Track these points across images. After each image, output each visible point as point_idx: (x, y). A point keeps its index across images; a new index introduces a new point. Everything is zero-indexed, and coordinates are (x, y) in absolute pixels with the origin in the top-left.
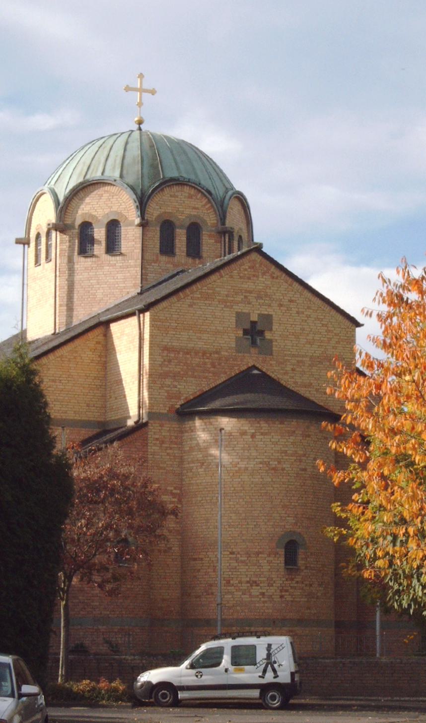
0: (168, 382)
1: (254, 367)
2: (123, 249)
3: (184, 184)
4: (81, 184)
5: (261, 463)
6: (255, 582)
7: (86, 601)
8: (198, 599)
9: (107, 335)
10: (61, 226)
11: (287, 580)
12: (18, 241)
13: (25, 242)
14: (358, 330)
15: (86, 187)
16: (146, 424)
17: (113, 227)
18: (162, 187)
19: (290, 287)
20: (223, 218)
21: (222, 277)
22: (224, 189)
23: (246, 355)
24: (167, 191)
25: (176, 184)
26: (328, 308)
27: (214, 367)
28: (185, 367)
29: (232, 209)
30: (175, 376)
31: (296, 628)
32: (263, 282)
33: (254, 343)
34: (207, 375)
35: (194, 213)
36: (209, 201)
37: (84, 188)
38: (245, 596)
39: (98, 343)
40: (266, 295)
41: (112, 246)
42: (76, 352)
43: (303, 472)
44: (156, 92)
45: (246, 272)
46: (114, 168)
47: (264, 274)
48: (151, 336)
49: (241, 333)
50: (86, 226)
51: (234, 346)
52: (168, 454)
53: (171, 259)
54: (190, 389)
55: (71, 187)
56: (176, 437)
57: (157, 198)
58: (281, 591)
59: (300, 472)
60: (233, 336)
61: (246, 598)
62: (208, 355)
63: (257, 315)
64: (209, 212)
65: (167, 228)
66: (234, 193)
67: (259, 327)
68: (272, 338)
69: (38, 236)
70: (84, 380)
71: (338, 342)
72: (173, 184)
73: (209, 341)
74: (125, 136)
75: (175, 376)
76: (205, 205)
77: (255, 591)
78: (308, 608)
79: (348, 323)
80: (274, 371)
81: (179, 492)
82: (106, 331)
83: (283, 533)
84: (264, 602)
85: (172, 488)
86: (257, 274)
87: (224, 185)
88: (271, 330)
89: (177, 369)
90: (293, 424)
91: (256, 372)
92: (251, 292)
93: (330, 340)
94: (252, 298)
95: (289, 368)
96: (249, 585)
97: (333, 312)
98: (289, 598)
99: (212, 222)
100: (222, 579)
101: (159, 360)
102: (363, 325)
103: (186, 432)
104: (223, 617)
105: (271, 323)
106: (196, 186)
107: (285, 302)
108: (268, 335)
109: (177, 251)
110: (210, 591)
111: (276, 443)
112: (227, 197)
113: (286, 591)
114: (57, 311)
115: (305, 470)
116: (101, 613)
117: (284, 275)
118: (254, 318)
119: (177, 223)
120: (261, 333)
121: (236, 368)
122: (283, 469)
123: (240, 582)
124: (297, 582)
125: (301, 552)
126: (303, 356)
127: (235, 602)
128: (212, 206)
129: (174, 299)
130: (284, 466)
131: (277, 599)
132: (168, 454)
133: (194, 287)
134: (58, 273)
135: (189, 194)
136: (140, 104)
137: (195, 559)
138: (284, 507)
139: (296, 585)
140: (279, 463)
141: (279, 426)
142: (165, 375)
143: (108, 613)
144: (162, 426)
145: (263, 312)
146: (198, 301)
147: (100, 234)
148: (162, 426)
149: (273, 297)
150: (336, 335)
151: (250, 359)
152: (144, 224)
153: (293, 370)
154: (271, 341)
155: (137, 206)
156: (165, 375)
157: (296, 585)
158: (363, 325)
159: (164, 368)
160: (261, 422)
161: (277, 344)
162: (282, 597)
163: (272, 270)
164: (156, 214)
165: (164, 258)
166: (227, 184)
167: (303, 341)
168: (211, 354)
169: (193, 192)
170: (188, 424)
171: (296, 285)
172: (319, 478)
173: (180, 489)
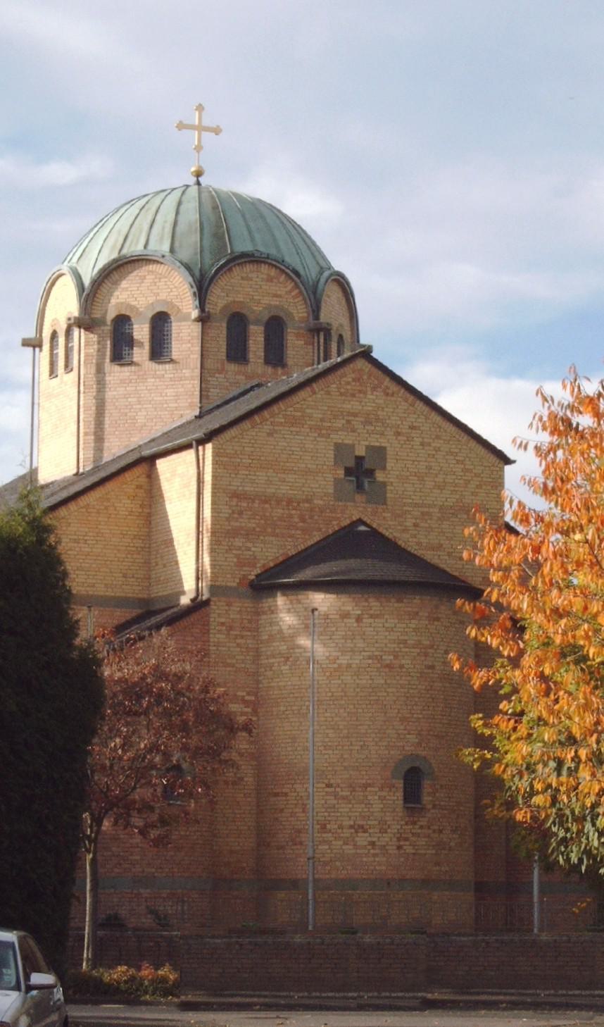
0: (238, 542)
1: (360, 522)
2: (175, 354)
3: (261, 262)
4: (115, 261)
5: (370, 658)
6: (362, 827)
8: (281, 851)
9: (152, 476)
10: (86, 321)
11: (406, 824)
12: (26, 343)
13: (35, 344)
14: (507, 468)
17: (160, 322)
19: (411, 408)
20: (316, 310)
21: (314, 393)
22: (317, 269)
24: (237, 271)
28: (263, 522)
30: (249, 534)
32: (373, 400)
33: (360, 487)
34: (293, 532)
35: (275, 302)
36: (296, 286)
37: (119, 267)
38: (347, 847)
40: (377, 420)
41: (159, 350)
42: (108, 500)
45: (349, 387)
46: (161, 239)
48: (214, 477)
49: (341, 473)
50: (122, 322)
52: (238, 645)
53: (242, 368)
54: (269, 552)
55: (100, 265)
56: (250, 621)
57: (223, 282)
58: (399, 840)
59: (425, 671)
60: (330, 477)
61: (349, 849)
62: (295, 504)
64: (296, 300)
65: (237, 323)
67: (367, 465)
68: (386, 480)
69: (54, 335)
70: (119, 540)
71: (479, 487)
72: (245, 262)
73: (297, 484)
74: (177, 194)
75: (249, 534)
76: (290, 292)
77: (362, 839)
78: (437, 864)
79: (493, 459)
80: (389, 526)
81: (253, 698)
84: (375, 855)
85: (245, 694)
86: (364, 389)
87: (318, 263)
88: (384, 468)
91: (362, 528)
92: (355, 415)
94: (357, 423)
95: (409, 523)
96: (353, 831)
97: (473, 444)
98: (409, 850)
99: (301, 315)
100: (315, 822)
101: (226, 511)
102: (514, 462)
103: (264, 613)
106: (278, 265)
107: (405, 429)
108: (380, 476)
109: (251, 356)
110: (298, 839)
112: (322, 280)
113: (406, 839)
114: (81, 442)
115: (432, 667)
116: (143, 871)
117: (403, 391)
118: (360, 451)
119: (251, 317)
120: (370, 473)
121: (335, 523)
122: (402, 667)
123: (341, 827)
124: (421, 827)
125: (427, 784)
126: (429, 506)
129: (246, 425)
130: (403, 662)
131: (392, 850)
132: (238, 645)
133: (275, 408)
135: (269, 275)
136: (199, 148)
137: (276, 795)
138: (403, 720)
139: (419, 831)
140: (396, 657)
142: (234, 533)
143: (153, 870)
144: (229, 604)
145: (372, 444)
147: (141, 332)
148: (229, 604)
151: (354, 510)
152: (204, 319)
153: (416, 525)
154: (384, 484)
156: (234, 533)
157: (419, 831)
158: (514, 462)
159: (232, 523)
161: (392, 488)
162: (399, 848)
163: (386, 383)
164: (221, 303)
165: (232, 367)
168: (298, 503)
169: (273, 272)
170: (267, 603)
171: (420, 405)
172: (452, 679)
173: (256, 696)
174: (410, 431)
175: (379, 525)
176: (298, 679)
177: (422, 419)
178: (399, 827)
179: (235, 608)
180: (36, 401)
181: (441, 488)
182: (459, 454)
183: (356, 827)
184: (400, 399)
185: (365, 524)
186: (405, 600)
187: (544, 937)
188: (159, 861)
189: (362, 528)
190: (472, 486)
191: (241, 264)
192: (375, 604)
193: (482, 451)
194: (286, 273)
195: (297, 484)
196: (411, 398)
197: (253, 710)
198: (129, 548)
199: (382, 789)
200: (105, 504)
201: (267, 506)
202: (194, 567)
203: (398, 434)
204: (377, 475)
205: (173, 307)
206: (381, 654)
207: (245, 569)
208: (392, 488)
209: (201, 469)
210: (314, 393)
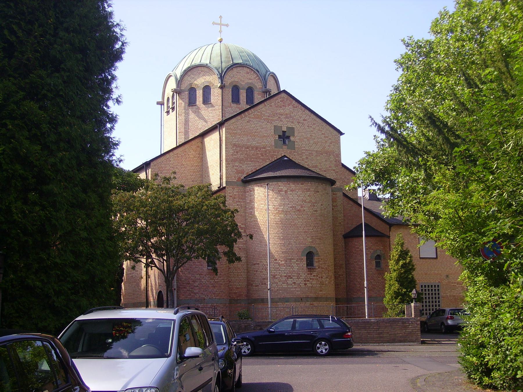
0: (237, 164)
1: (285, 156)
2: (212, 101)
3: (244, 67)
4: (189, 67)
5: (291, 207)
6: (290, 276)
7: (191, 290)
8: (257, 287)
9: (203, 143)
12: (158, 103)
14: (342, 137)
15: (192, 69)
17: (207, 90)
18: (233, 67)
19: (304, 113)
20: (265, 85)
21: (265, 106)
23: (280, 149)
25: (239, 66)
26: (325, 124)
28: (246, 156)
29: (270, 81)
30: (241, 161)
31: (314, 303)
32: (288, 109)
33: (284, 143)
34: (259, 160)
35: (250, 81)
36: (258, 76)
37: (190, 70)
38: (284, 285)
39: (199, 147)
40: (291, 117)
41: (206, 100)
42: (186, 152)
43: (316, 212)
44: (229, 26)
45: (279, 104)
46: (206, 59)
47: (289, 105)
48: (226, 138)
49: (277, 137)
50: (192, 91)
51: (274, 144)
52: (238, 205)
53: (238, 106)
54: (249, 168)
55: (184, 69)
56: (242, 195)
57: (230, 73)
59: (314, 212)
61: (285, 286)
62: (259, 149)
63: (286, 128)
64: (258, 81)
65: (236, 90)
66: (270, 73)
67: (287, 134)
68: (294, 140)
70: (193, 173)
71: (331, 143)
72: (238, 66)
73: (258, 131)
74: (211, 46)
75: (241, 161)
76: (255, 78)
77: (290, 281)
79: (335, 132)
80: (296, 159)
81: (244, 226)
82: (202, 140)
83: (305, 247)
84: (295, 288)
85: (241, 224)
86: (285, 105)
87: (266, 69)
88: (294, 136)
89: (242, 157)
90: (308, 185)
91: (286, 159)
92: (282, 115)
93: (326, 142)
94: (282, 117)
95: (304, 157)
96: (286, 278)
97: (328, 127)
99: (259, 87)
100: (271, 275)
101: (231, 151)
102: (344, 134)
103: (248, 192)
104: (272, 297)
105: (294, 132)
106: (250, 67)
107: (301, 120)
108: (292, 138)
109: (241, 101)
110: (264, 282)
111: (299, 196)
112: (267, 75)
113: (308, 281)
114: (178, 136)
115: (316, 211)
116: (200, 297)
117: (300, 106)
118: (284, 129)
119: (241, 87)
120: (288, 137)
121: (275, 157)
122: (304, 210)
123: (281, 276)
124: (314, 276)
125: (316, 258)
126: (312, 151)
127: (278, 288)
128: (259, 78)
129: (238, 117)
130: (305, 209)
131: (302, 285)
132: (238, 205)
134: (178, 116)
135: (247, 72)
136: (220, 32)
137: (255, 264)
138: (305, 232)
139: (313, 277)
140: (302, 207)
141: (301, 186)
142: (235, 160)
143: (204, 296)
144: (233, 189)
145: (289, 126)
146: (253, 119)
147: (199, 94)
148: (233, 189)
149: (294, 117)
150: (330, 139)
151: (283, 151)
152: (222, 87)
153: (307, 158)
154: (294, 142)
155: (219, 77)
156: (235, 160)
157: (313, 277)
158: (344, 134)
159: (234, 156)
160: (291, 184)
161: (297, 143)
162: (305, 284)
163: (293, 103)
164: (229, 82)
166: (267, 69)
167: (312, 142)
168: (260, 149)
169: (248, 70)
170: (250, 187)
171: (307, 112)
172: (324, 216)
173: (245, 225)
174: (303, 121)
175: (292, 157)
176: (265, 270)
177: (308, 117)
178: (305, 276)
179: (236, 190)
180: (162, 124)
181: (316, 143)
182: (323, 131)
183: (288, 276)
184: (299, 109)
185: (287, 157)
186: (304, 184)
187: (373, 320)
188: (206, 292)
189: (286, 159)
190: (328, 144)
191: (236, 67)
192: (292, 186)
194: (254, 71)
195: (258, 131)
196: (303, 109)
197: (244, 231)
198: (194, 170)
199: (297, 261)
200: (184, 153)
201: (248, 150)
202: (219, 175)
203: (299, 123)
204: (291, 138)
205: (211, 83)
206: (295, 205)
207: (239, 174)
208: (297, 143)
209: (221, 136)
210: (265, 106)
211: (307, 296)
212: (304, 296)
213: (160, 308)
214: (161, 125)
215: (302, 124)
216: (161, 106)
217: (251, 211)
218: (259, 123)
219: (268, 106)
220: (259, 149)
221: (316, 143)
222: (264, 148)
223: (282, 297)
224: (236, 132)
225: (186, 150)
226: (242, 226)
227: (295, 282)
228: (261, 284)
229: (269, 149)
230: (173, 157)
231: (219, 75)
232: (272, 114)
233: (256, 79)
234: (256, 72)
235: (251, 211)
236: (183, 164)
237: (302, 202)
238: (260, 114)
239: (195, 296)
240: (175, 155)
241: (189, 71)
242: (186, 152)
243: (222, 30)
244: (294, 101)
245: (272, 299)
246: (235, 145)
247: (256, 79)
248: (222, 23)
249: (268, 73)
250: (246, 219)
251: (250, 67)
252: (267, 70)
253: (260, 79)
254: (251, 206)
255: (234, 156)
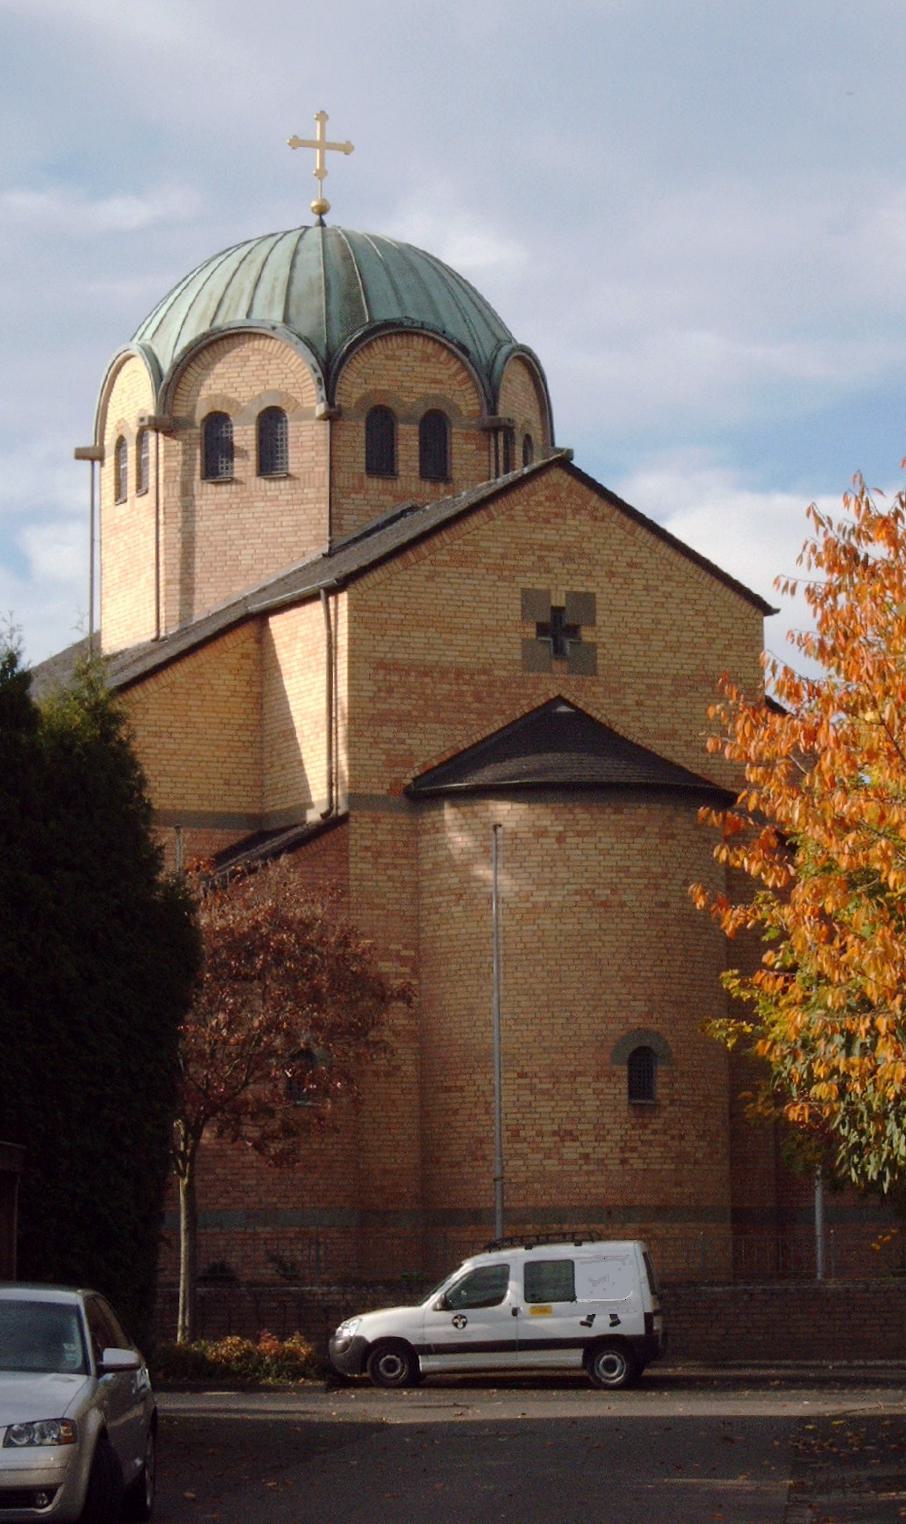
0: (387, 732)
1: (561, 700)
4: (205, 336)
5: (577, 893)
6: (570, 1133)
8: (455, 1170)
9: (264, 641)
10: (165, 423)
11: (633, 1128)
12: (81, 455)
14: (767, 620)
16: (344, 819)
17: (271, 422)
19: (629, 537)
20: (492, 401)
21: (492, 518)
22: (494, 342)
23: (543, 675)
25: (396, 334)
27: (479, 700)
28: (421, 702)
30: (402, 720)
32: (575, 526)
33: (558, 651)
35: (434, 390)
36: (464, 367)
37: (211, 344)
40: (582, 555)
41: (270, 461)
42: (201, 675)
43: (664, 910)
44: (352, 148)
45: (540, 509)
48: (352, 640)
49: (532, 631)
53: (389, 485)
54: (431, 745)
55: (184, 342)
56: (406, 844)
57: (359, 362)
58: (622, 1150)
60: (516, 638)
61: (552, 1165)
63: (564, 596)
64: (464, 387)
65: (381, 422)
66: (513, 350)
67: (568, 620)
68: (595, 640)
69: (121, 443)
71: (728, 647)
72: (390, 334)
75: (402, 720)
76: (455, 375)
77: (571, 1151)
78: (678, 1184)
79: (746, 607)
80: (600, 705)
81: (413, 953)
84: (588, 1173)
85: (400, 947)
87: (494, 334)
88: (593, 623)
91: (563, 709)
92: (550, 549)
95: (630, 700)
96: (557, 1138)
97: (718, 586)
98: (638, 1164)
99: (471, 408)
100: (504, 1128)
101: (370, 688)
103: (426, 832)
106: (437, 337)
108: (587, 635)
109: (401, 467)
111: (606, 853)
113: (633, 1150)
114: (162, 594)
115: (666, 905)
116: (261, 1202)
117: (617, 513)
118: (559, 600)
119: (400, 412)
120: (573, 631)
121: (523, 702)
122: (622, 904)
123: (540, 1134)
124: (654, 1132)
125: (661, 1069)
126: (658, 676)
128: (470, 376)
129: (396, 565)
130: (625, 898)
133: (436, 541)
134: (161, 517)
135: (424, 352)
137: (448, 1089)
138: (626, 979)
140: (614, 891)
141: (613, 817)
142: (381, 719)
146: (446, 569)
148: (376, 821)
150: (725, 631)
151: (552, 684)
152: (333, 416)
153: (638, 704)
154: (593, 646)
156: (381, 719)
157: (652, 1137)
159: (378, 706)
162: (624, 1161)
165: (375, 484)
169: (430, 348)
170: (429, 818)
171: (642, 533)
173: (417, 949)
174: (628, 570)
180: (97, 538)
181: (674, 649)
185: (566, 703)
189: (563, 709)
190: (718, 646)
192: (583, 817)
193: (731, 596)
199: (597, 1078)
201: (427, 680)
211: (545, 1311)
212: (619, 1203)
213: (733, 1395)
214: (92, 540)
215: (621, 580)
216: (93, 464)
217: (438, 900)
218: (467, 581)
219: (502, 517)
220: (467, 677)
221: (674, 649)
222: (485, 672)
223: (543, 1204)
224: (386, 616)
225: (202, 670)
226: (404, 953)
227: (588, 1155)
228: (469, 1159)
229: (504, 673)
230: (156, 695)
231: (319, 369)
232: (513, 546)
233: (459, 378)
234: (459, 353)
235: (438, 900)
236: (194, 720)
237: (614, 875)
238: (472, 548)
239: (246, 1199)
240: (164, 690)
241: (206, 347)
242: (201, 675)
243: (327, 167)
244: (596, 497)
245: (505, 1210)
246: (381, 665)
247: (459, 378)
248: (327, 140)
249: (506, 349)
250: (419, 930)
251: (437, 337)
252: (500, 336)
253: (474, 382)
254: (438, 882)
255: (378, 706)
